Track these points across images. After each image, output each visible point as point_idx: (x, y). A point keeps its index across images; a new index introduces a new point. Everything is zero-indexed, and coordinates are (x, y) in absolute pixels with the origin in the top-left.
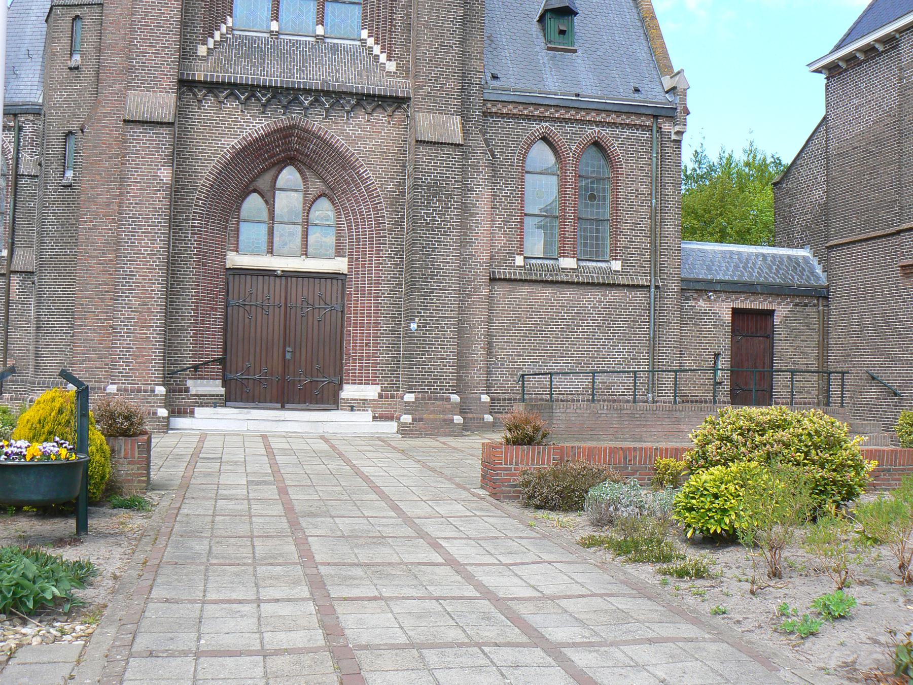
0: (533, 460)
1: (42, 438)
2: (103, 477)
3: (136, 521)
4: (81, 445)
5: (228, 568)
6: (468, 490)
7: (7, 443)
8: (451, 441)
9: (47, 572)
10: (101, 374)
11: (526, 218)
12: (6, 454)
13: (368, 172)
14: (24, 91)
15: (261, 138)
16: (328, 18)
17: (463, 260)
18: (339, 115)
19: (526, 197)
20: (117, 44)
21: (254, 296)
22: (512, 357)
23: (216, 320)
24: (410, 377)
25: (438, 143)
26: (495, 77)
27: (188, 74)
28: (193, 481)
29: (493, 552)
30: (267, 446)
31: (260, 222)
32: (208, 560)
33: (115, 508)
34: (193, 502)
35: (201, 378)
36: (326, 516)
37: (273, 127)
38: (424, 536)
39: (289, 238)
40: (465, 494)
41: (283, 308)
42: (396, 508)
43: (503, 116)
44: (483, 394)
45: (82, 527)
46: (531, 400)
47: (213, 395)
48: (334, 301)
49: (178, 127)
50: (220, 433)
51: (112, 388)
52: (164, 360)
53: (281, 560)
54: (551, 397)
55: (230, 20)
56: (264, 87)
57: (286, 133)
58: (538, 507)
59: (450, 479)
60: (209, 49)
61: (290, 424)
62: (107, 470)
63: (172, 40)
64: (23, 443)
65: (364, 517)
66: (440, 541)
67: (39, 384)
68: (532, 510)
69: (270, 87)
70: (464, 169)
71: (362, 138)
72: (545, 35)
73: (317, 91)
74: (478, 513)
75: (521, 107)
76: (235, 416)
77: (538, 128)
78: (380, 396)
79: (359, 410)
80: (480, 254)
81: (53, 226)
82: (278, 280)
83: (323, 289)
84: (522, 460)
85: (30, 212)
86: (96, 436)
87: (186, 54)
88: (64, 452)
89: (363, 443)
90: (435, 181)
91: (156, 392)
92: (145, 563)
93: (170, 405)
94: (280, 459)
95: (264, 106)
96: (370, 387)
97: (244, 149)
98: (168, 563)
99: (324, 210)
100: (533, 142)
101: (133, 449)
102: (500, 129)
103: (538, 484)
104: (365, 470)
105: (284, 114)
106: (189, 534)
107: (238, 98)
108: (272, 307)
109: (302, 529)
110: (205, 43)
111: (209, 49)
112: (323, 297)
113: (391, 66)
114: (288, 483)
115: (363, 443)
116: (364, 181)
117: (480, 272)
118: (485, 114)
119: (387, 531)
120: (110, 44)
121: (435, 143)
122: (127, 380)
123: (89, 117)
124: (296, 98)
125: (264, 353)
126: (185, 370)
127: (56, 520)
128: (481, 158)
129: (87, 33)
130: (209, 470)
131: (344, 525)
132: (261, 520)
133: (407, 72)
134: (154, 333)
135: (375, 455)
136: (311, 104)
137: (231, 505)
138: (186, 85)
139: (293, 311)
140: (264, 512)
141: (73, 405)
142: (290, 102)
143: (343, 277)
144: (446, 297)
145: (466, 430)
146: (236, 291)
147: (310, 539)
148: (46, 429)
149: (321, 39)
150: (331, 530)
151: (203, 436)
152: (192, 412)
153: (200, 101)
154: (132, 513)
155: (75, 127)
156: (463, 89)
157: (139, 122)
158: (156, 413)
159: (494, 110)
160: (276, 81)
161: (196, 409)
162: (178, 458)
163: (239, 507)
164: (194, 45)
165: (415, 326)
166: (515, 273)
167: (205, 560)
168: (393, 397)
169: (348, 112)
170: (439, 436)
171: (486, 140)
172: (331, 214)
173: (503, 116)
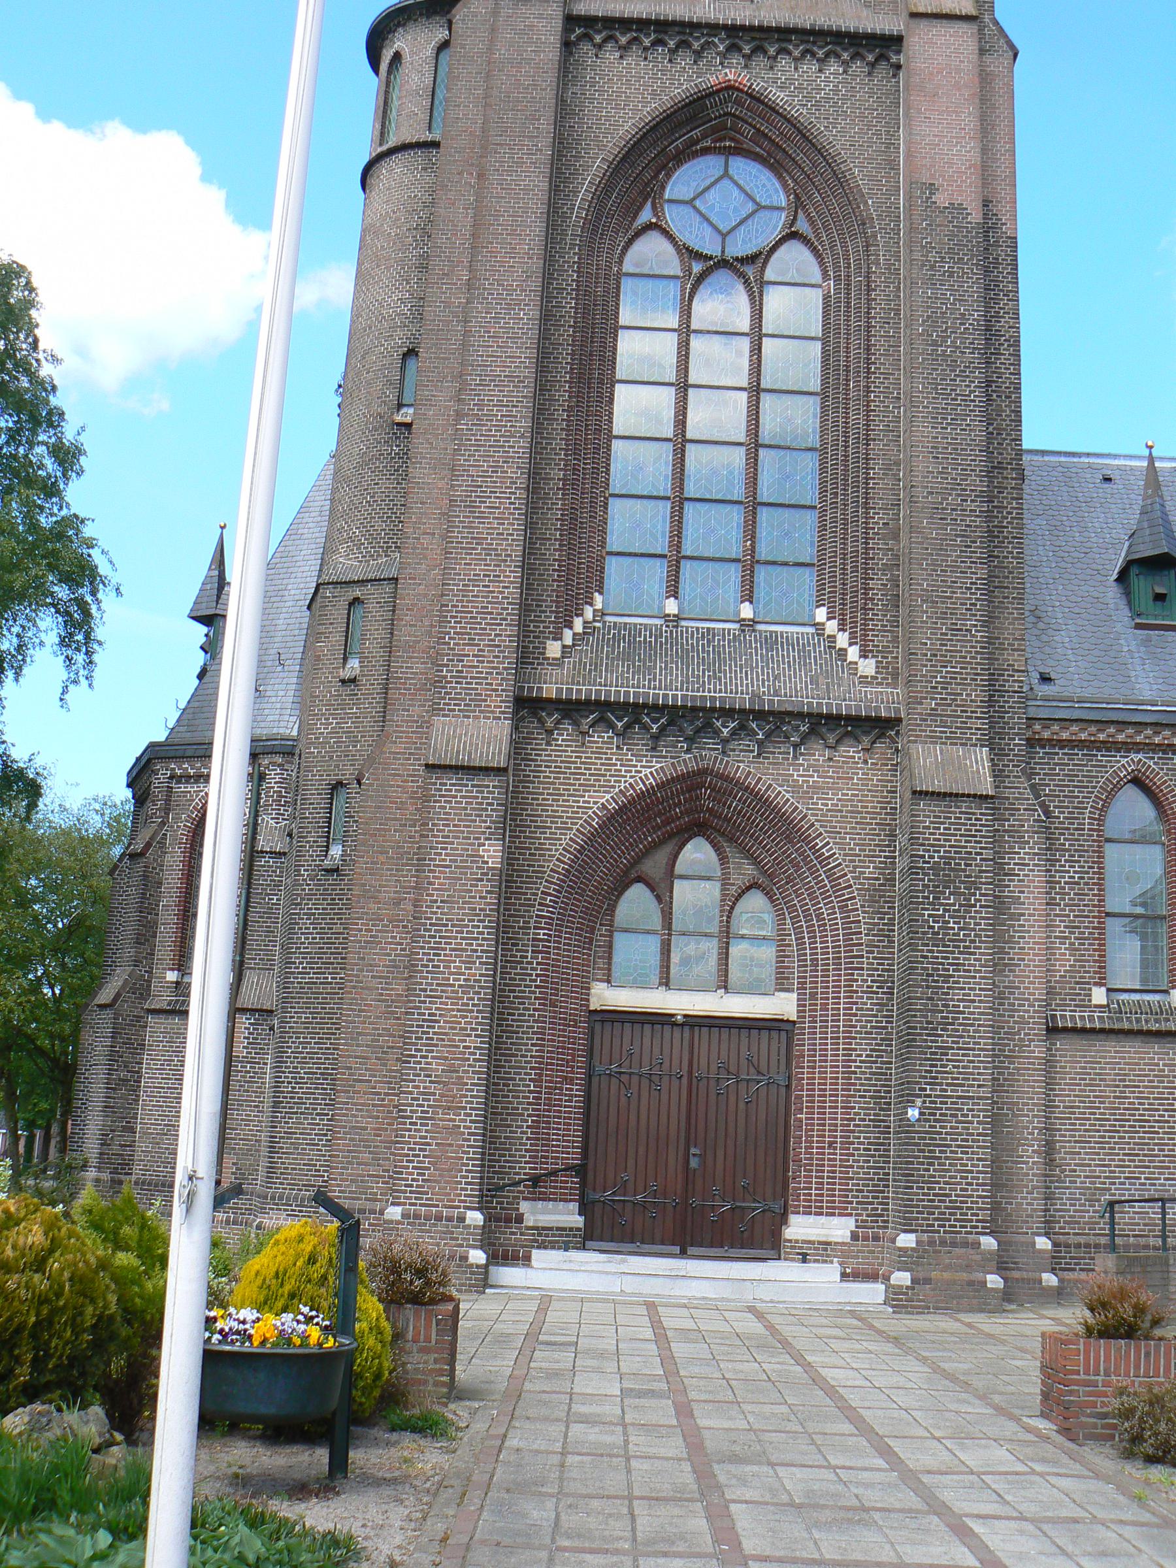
0: (1137, 1367)
1: (280, 1304)
2: (378, 1376)
3: (429, 1457)
4: (343, 1319)
5: (588, 1557)
6: (1018, 1420)
7: (221, 1312)
8: (981, 1321)
9: (280, 1552)
10: (377, 1187)
11: (1109, 920)
12: (221, 1331)
13: (828, 846)
14: (270, 718)
15: (651, 792)
16: (760, 592)
17: (999, 997)
18: (780, 751)
19: (1107, 884)
20: (419, 642)
21: (636, 1058)
22: (1089, 1168)
23: (572, 1098)
24: (908, 1205)
25: (951, 795)
26: (1045, 679)
27: (531, 689)
28: (528, 1386)
29: (1070, 1548)
30: (657, 1324)
31: (648, 932)
32: (553, 1540)
33: (393, 1430)
34: (527, 1425)
35: (545, 1198)
36: (760, 1463)
37: (671, 772)
38: (940, 1509)
39: (698, 963)
40: (1012, 1427)
41: (685, 1081)
42: (886, 1452)
43: (1062, 744)
44: (1039, 1235)
45: (339, 1464)
46: (1127, 1247)
47: (564, 1229)
48: (773, 1069)
49: (513, 776)
50: (573, 1299)
51: (394, 1213)
52: (482, 1166)
53: (681, 1547)
54: (1164, 1242)
55: (598, 600)
56: (655, 707)
57: (691, 782)
58: (1151, 1460)
59: (983, 1397)
60: (564, 647)
61: (694, 1283)
62: (386, 1364)
63: (507, 634)
64: (248, 1314)
65: (829, 1467)
66: (970, 1523)
67: (273, 1198)
68: (1139, 1464)
69: (665, 706)
70: (996, 838)
71: (818, 788)
72: (1129, 603)
73: (742, 711)
74: (1038, 1468)
75: (1093, 729)
76: (600, 1267)
77: (1125, 763)
78: (854, 1236)
79: (816, 1261)
80: (1030, 987)
81: (307, 938)
82: (677, 1031)
83: (754, 1049)
84: (1117, 1367)
85: (270, 911)
86: (370, 1306)
87: (527, 655)
88: (315, 1333)
89: (824, 1321)
90: (947, 860)
91: (467, 1222)
92: (444, 1540)
93: (490, 1244)
94: (680, 1349)
95: (656, 738)
96: (835, 1220)
97: (622, 809)
98: (483, 1542)
99: (755, 902)
100: (1117, 788)
101: (428, 1327)
102: (1058, 769)
103: (1148, 1414)
104: (832, 1375)
105: (688, 751)
106: (517, 1488)
107: (611, 726)
108: (666, 1079)
109: (719, 1487)
110: (558, 637)
111: (564, 647)
112: (755, 1060)
113: (868, 667)
114: (693, 1395)
115: (824, 1321)
116: (824, 861)
117: (1029, 1015)
118: (1031, 743)
119: (873, 1497)
120: (407, 642)
121: (945, 795)
122: (420, 1207)
123: (371, 760)
124: (708, 725)
125: (651, 1158)
126: (518, 1183)
127: (295, 1449)
128: (1026, 819)
129: (372, 626)
130: (556, 1366)
131: (794, 1481)
132: (645, 1465)
133: (895, 675)
134: (467, 1121)
135: (847, 1345)
136: (734, 733)
137: (593, 1435)
138: (528, 707)
139: (704, 1083)
140: (652, 1451)
141: (333, 1250)
142: (698, 731)
143: (788, 1027)
144: (970, 1061)
145: (1009, 1301)
146: (606, 1051)
147: (733, 1507)
148: (287, 1288)
149: (748, 625)
150: (771, 1490)
151: (546, 1301)
152: (527, 1258)
153: (550, 732)
154: (422, 1442)
155: (348, 774)
156: (991, 702)
157: (451, 767)
158: (466, 1258)
159: (1046, 735)
160: (675, 697)
161: (534, 1252)
162: (503, 1340)
163: (608, 1439)
164: (541, 639)
165: (916, 1113)
166: (1091, 1019)
167: (548, 1540)
168: (876, 1238)
169: (796, 746)
170: (959, 1311)
171: (1033, 787)
172: (769, 917)
173: (1062, 744)
